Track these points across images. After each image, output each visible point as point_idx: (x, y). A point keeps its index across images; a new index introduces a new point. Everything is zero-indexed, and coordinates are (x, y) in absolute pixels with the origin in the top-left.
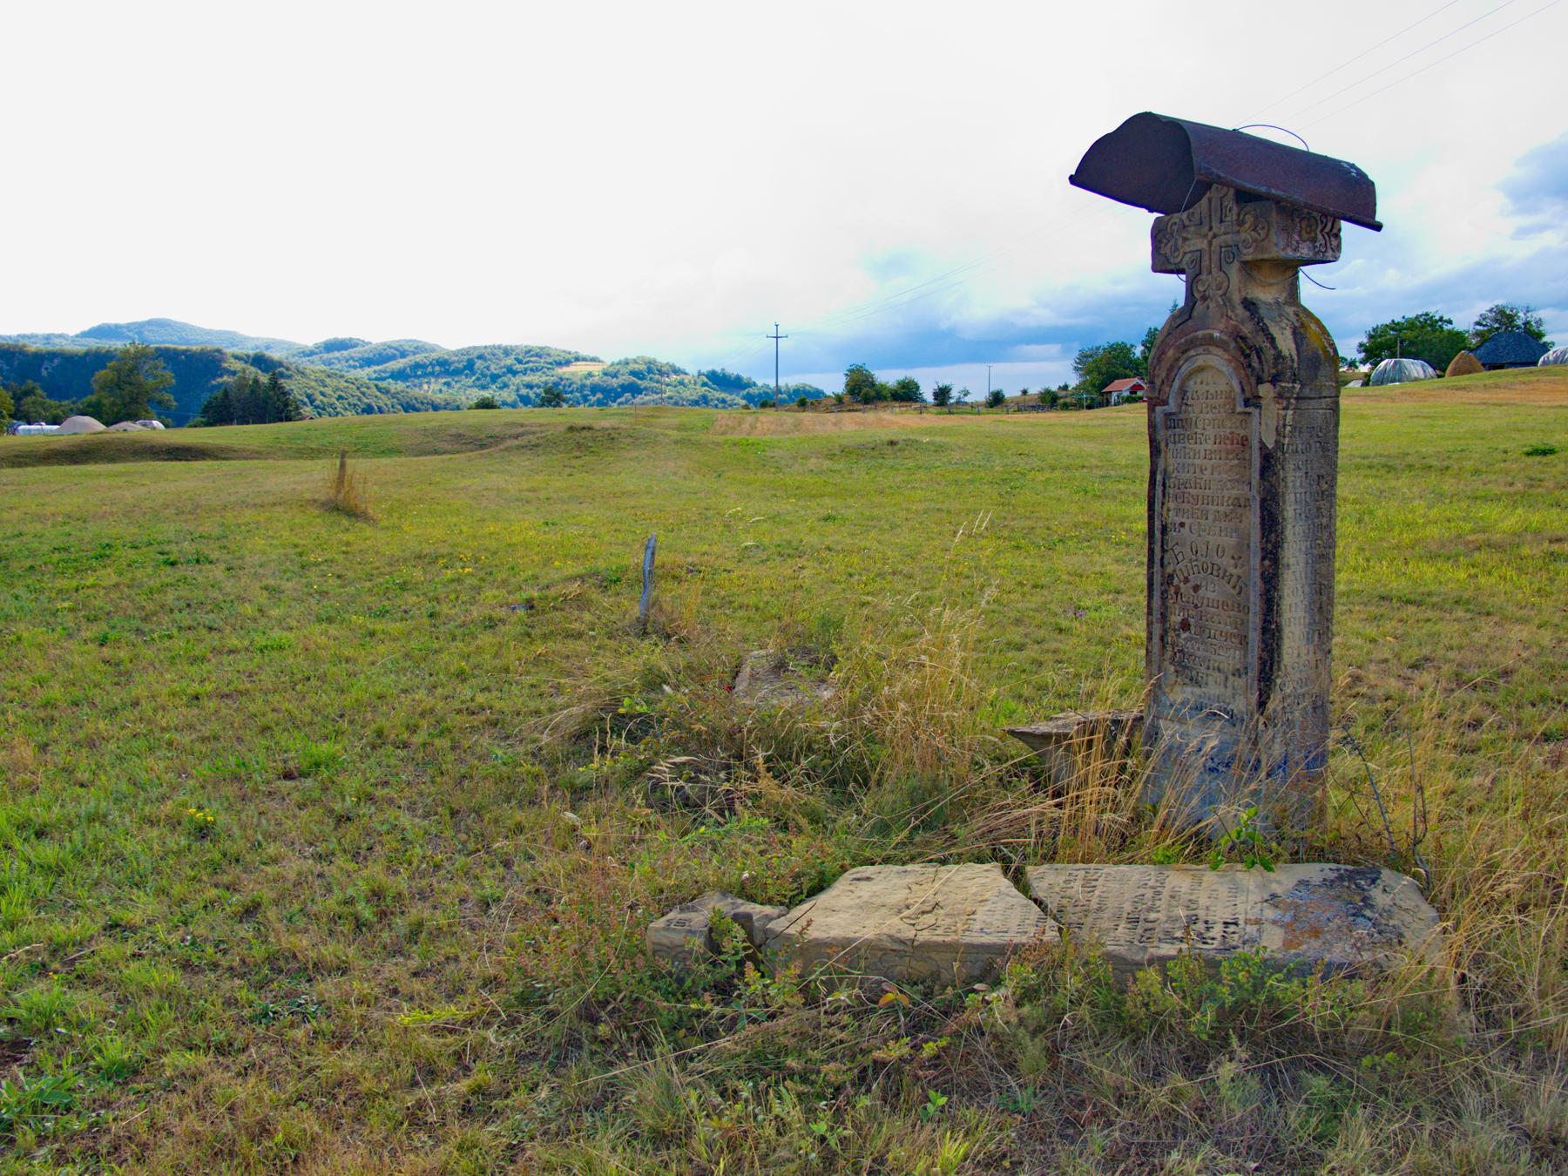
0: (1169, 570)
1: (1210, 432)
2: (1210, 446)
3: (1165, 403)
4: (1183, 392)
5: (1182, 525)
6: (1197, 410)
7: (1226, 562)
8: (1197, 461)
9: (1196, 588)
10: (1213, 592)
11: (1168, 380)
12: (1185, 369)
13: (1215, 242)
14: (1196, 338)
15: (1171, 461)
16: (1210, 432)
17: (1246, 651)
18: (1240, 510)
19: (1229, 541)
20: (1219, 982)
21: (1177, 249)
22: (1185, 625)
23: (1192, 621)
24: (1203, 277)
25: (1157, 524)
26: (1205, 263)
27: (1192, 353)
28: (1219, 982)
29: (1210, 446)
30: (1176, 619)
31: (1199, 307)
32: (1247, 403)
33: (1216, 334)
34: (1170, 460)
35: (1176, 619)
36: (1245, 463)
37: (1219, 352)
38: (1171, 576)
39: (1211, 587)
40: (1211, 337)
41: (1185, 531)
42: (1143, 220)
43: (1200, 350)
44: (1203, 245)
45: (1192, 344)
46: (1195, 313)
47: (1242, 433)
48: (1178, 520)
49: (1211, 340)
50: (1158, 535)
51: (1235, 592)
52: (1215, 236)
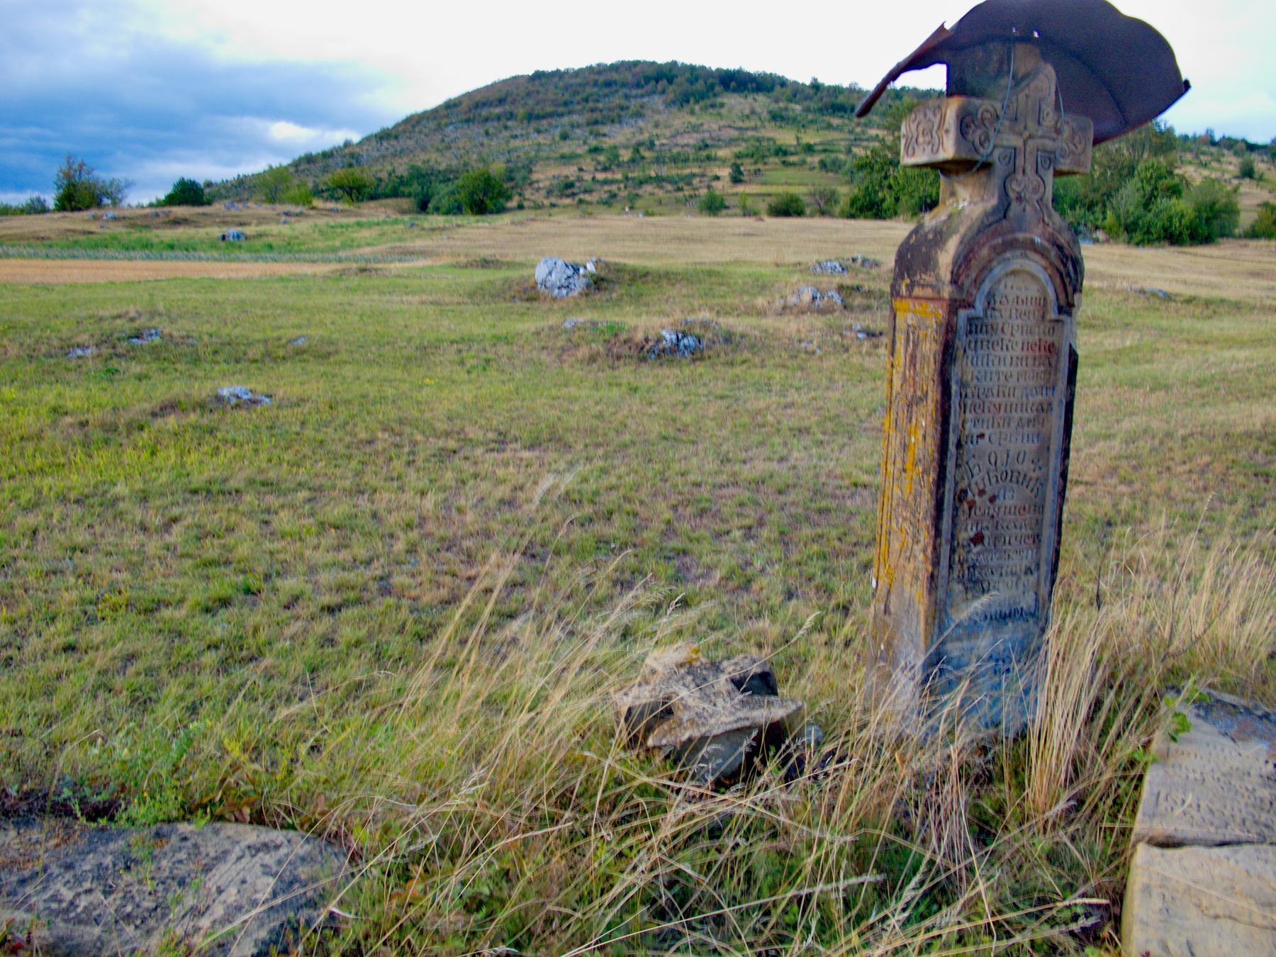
0: (963, 485)
1: (1018, 337)
2: (1017, 352)
3: (971, 305)
4: (991, 295)
5: (982, 436)
6: (1006, 314)
7: (1026, 467)
8: (1002, 368)
9: (993, 499)
10: (1011, 499)
11: (977, 282)
12: (998, 270)
13: (1030, 143)
14: (1016, 240)
15: (970, 369)
16: (1018, 337)
17: (1038, 548)
18: (1043, 415)
19: (1030, 447)
20: (809, 897)
21: (987, 138)
22: (978, 539)
23: (986, 533)
24: (1019, 176)
25: (952, 439)
26: (1020, 162)
27: (1008, 255)
28: (809, 897)
29: (1017, 352)
30: (964, 535)
31: (1015, 208)
32: (1060, 310)
33: (1038, 240)
34: (963, 369)
35: (964, 535)
36: (1052, 367)
37: (1037, 257)
38: (964, 492)
39: (1008, 495)
40: (1032, 242)
41: (984, 443)
42: (944, 88)
43: (1018, 253)
44: (1017, 142)
45: (1011, 245)
46: (1011, 214)
47: (1049, 339)
48: (976, 431)
49: (1032, 246)
50: (947, 445)
51: (1033, 495)
52: (1030, 137)
